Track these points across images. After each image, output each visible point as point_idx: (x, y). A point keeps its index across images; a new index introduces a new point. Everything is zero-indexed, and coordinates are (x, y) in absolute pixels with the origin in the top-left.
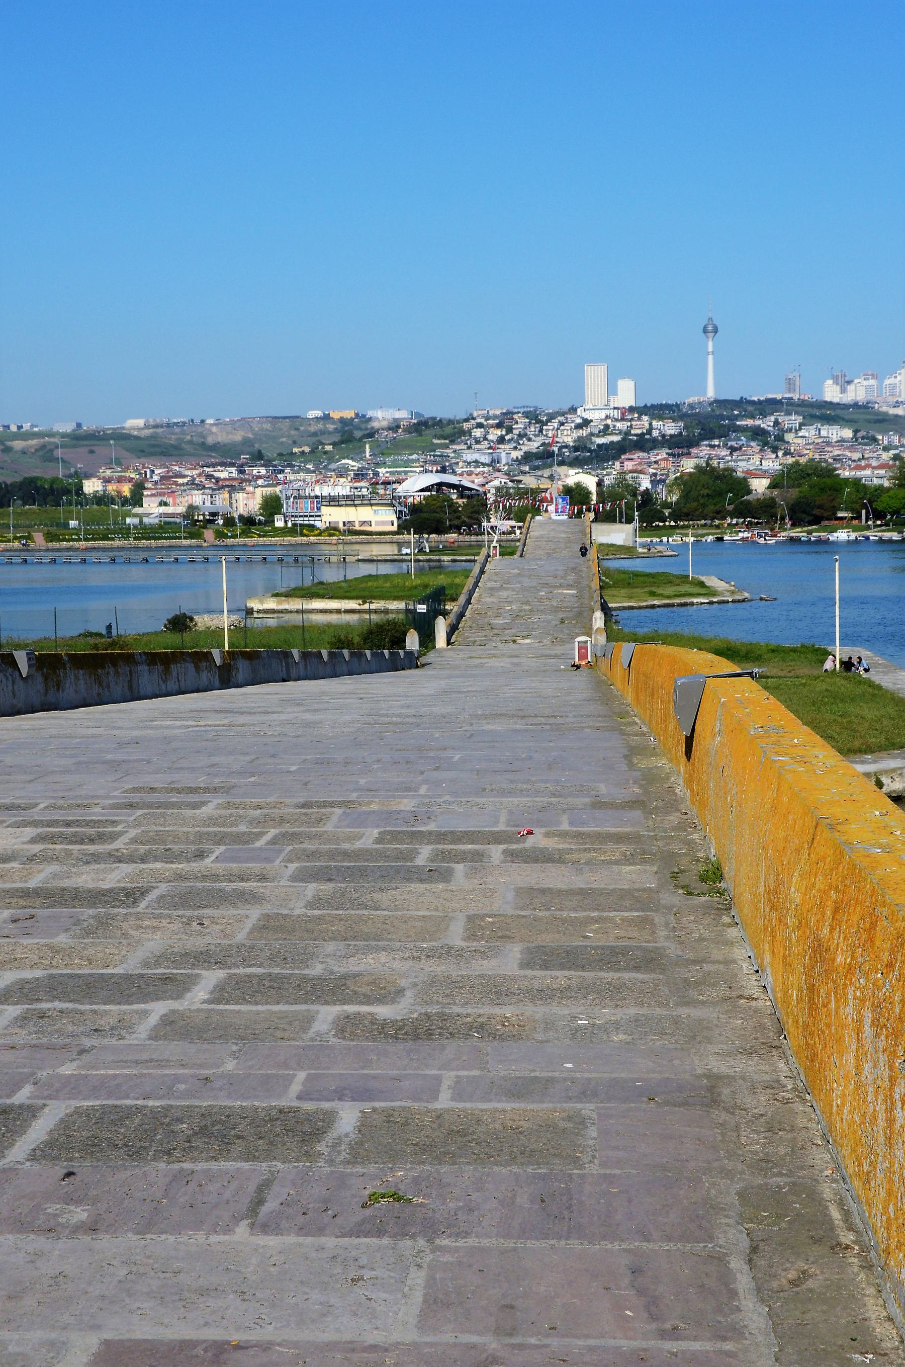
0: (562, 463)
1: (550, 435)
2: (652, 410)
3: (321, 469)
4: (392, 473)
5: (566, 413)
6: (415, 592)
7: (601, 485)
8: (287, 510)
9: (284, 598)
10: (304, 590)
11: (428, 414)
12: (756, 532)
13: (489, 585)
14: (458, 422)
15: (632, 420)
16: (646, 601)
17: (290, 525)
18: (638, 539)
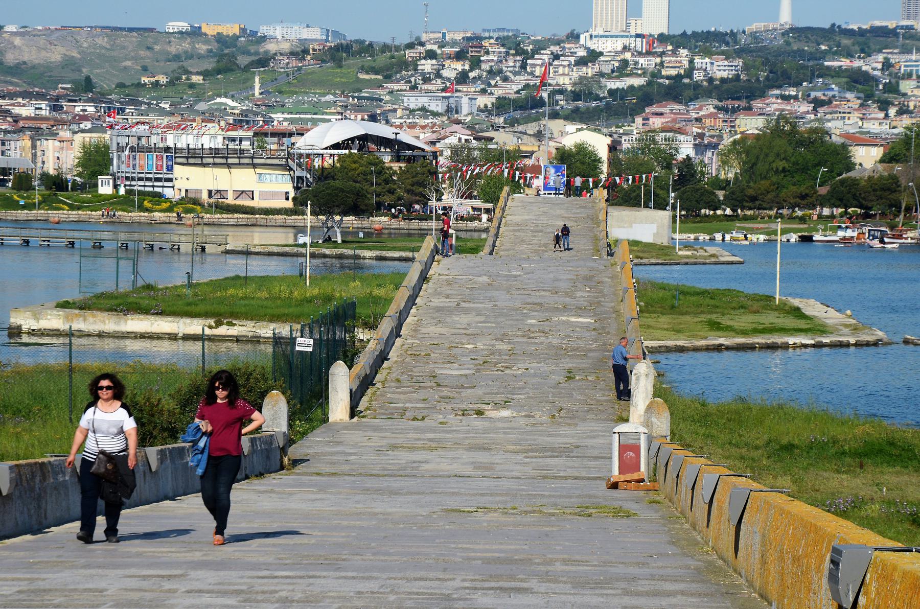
0: (554, 116)
1: (538, 73)
2: (693, 41)
3: (184, 109)
4: (292, 121)
5: (563, 42)
6: (307, 308)
7: (615, 149)
8: (119, 167)
9: (77, 311)
10: (116, 298)
11: (351, 35)
12: (866, 230)
13: (437, 302)
14: (398, 49)
15: (662, 54)
16: (706, 338)
17: (122, 191)
18: (677, 236)
